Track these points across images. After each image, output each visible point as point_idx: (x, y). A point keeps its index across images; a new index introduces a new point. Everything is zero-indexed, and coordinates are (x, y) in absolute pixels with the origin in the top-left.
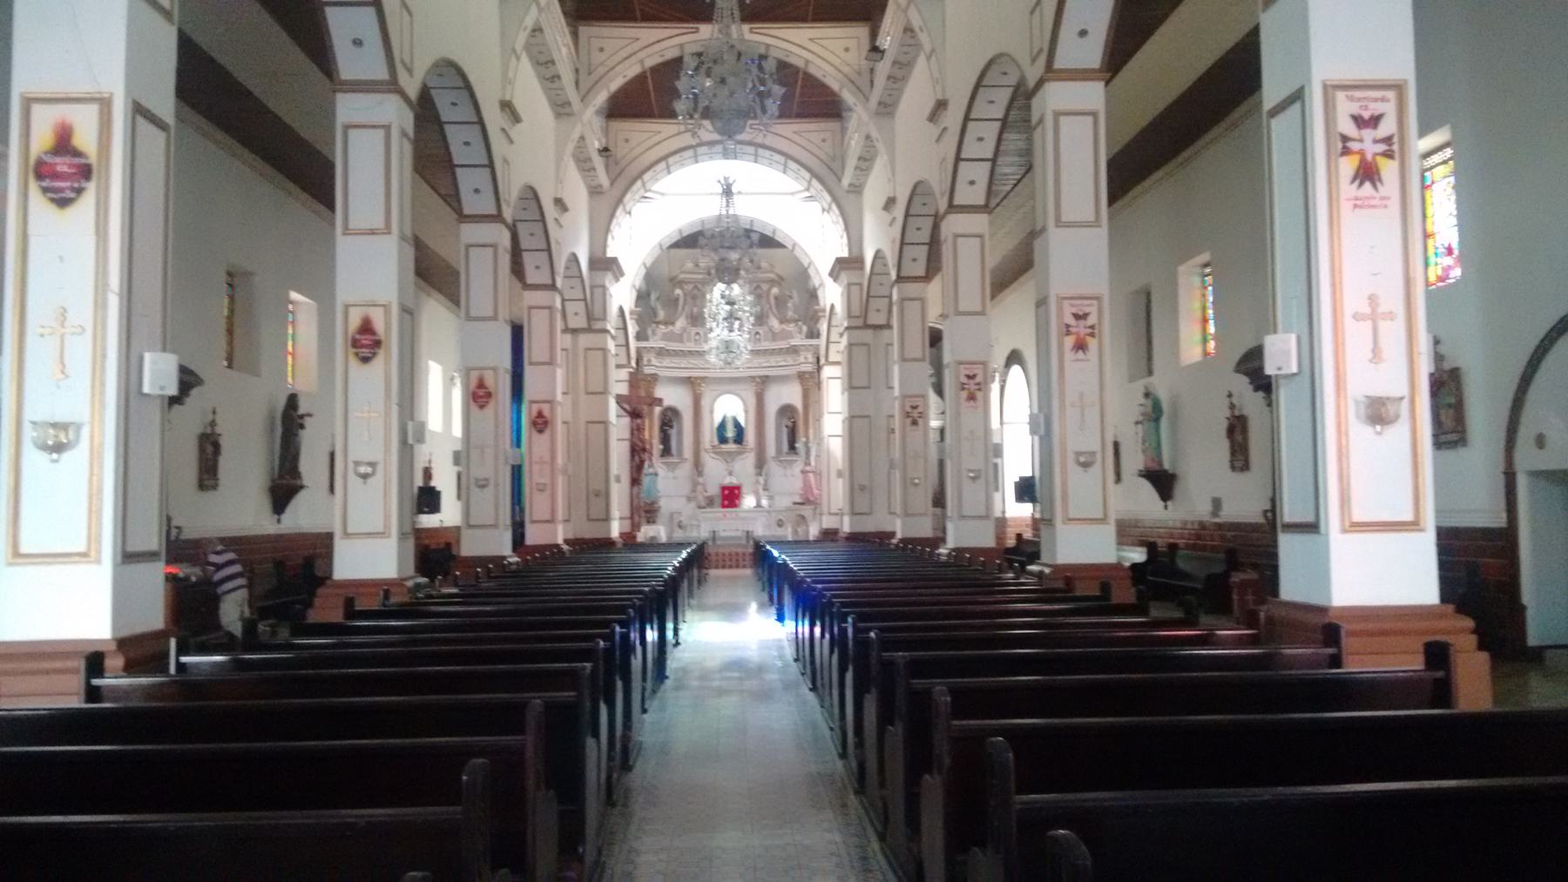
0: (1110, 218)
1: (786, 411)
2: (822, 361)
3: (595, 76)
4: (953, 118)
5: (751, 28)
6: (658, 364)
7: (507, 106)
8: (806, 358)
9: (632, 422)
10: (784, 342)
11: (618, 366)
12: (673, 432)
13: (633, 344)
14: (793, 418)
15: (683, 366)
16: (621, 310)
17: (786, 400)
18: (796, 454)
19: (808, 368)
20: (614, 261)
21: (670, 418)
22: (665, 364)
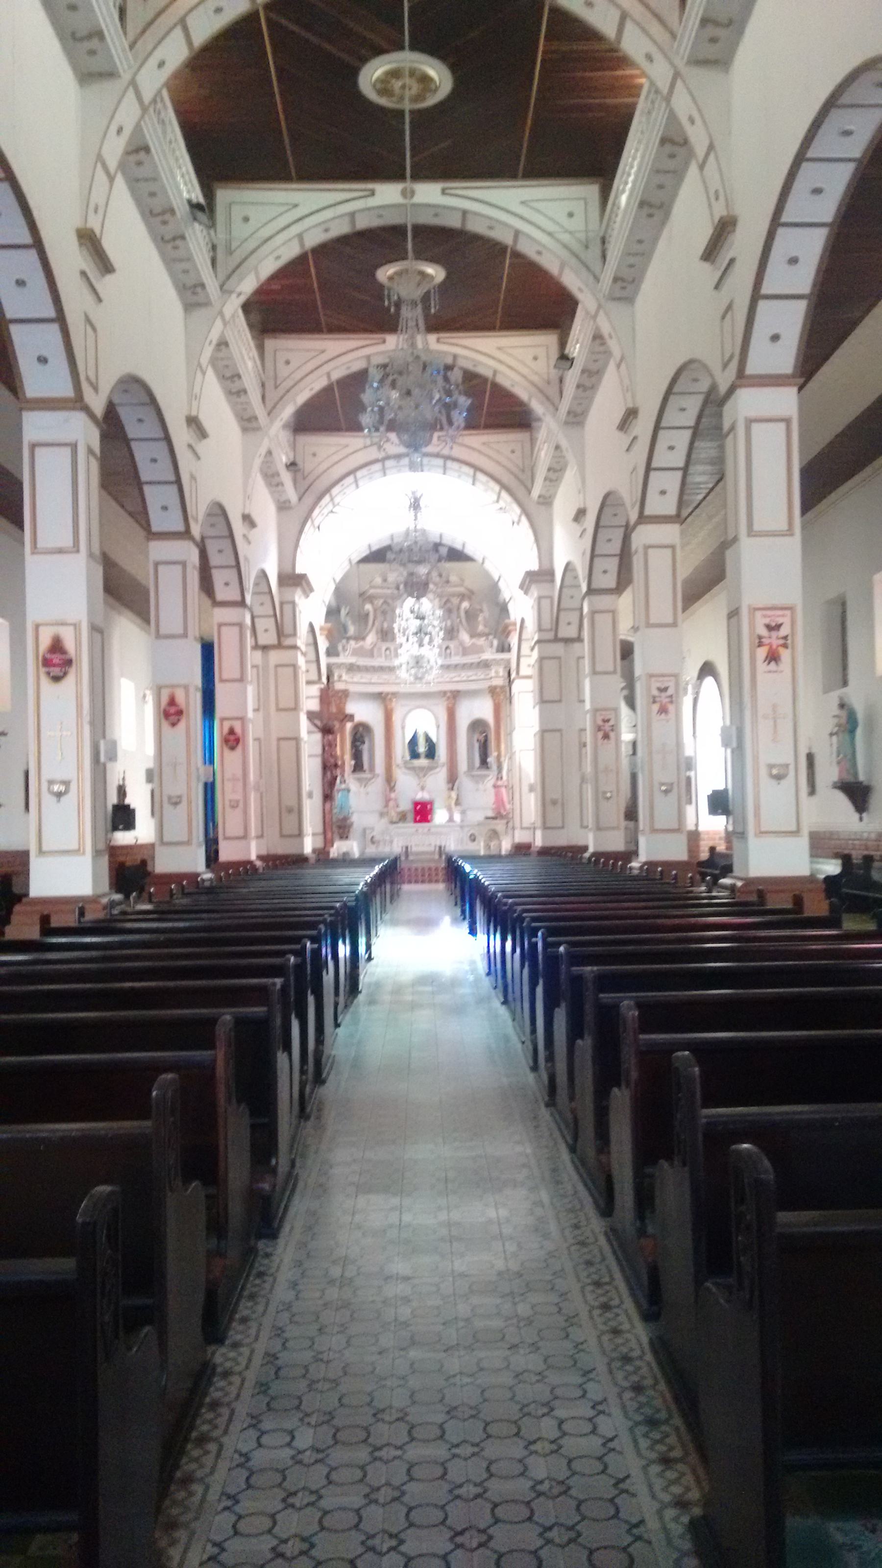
0: (804, 527)
1: (478, 726)
2: (513, 675)
7: (193, 422)
9: (323, 737)
11: (309, 683)
12: (365, 748)
13: (324, 660)
18: (488, 768)
19: (499, 682)
21: (361, 733)
22: (355, 680)
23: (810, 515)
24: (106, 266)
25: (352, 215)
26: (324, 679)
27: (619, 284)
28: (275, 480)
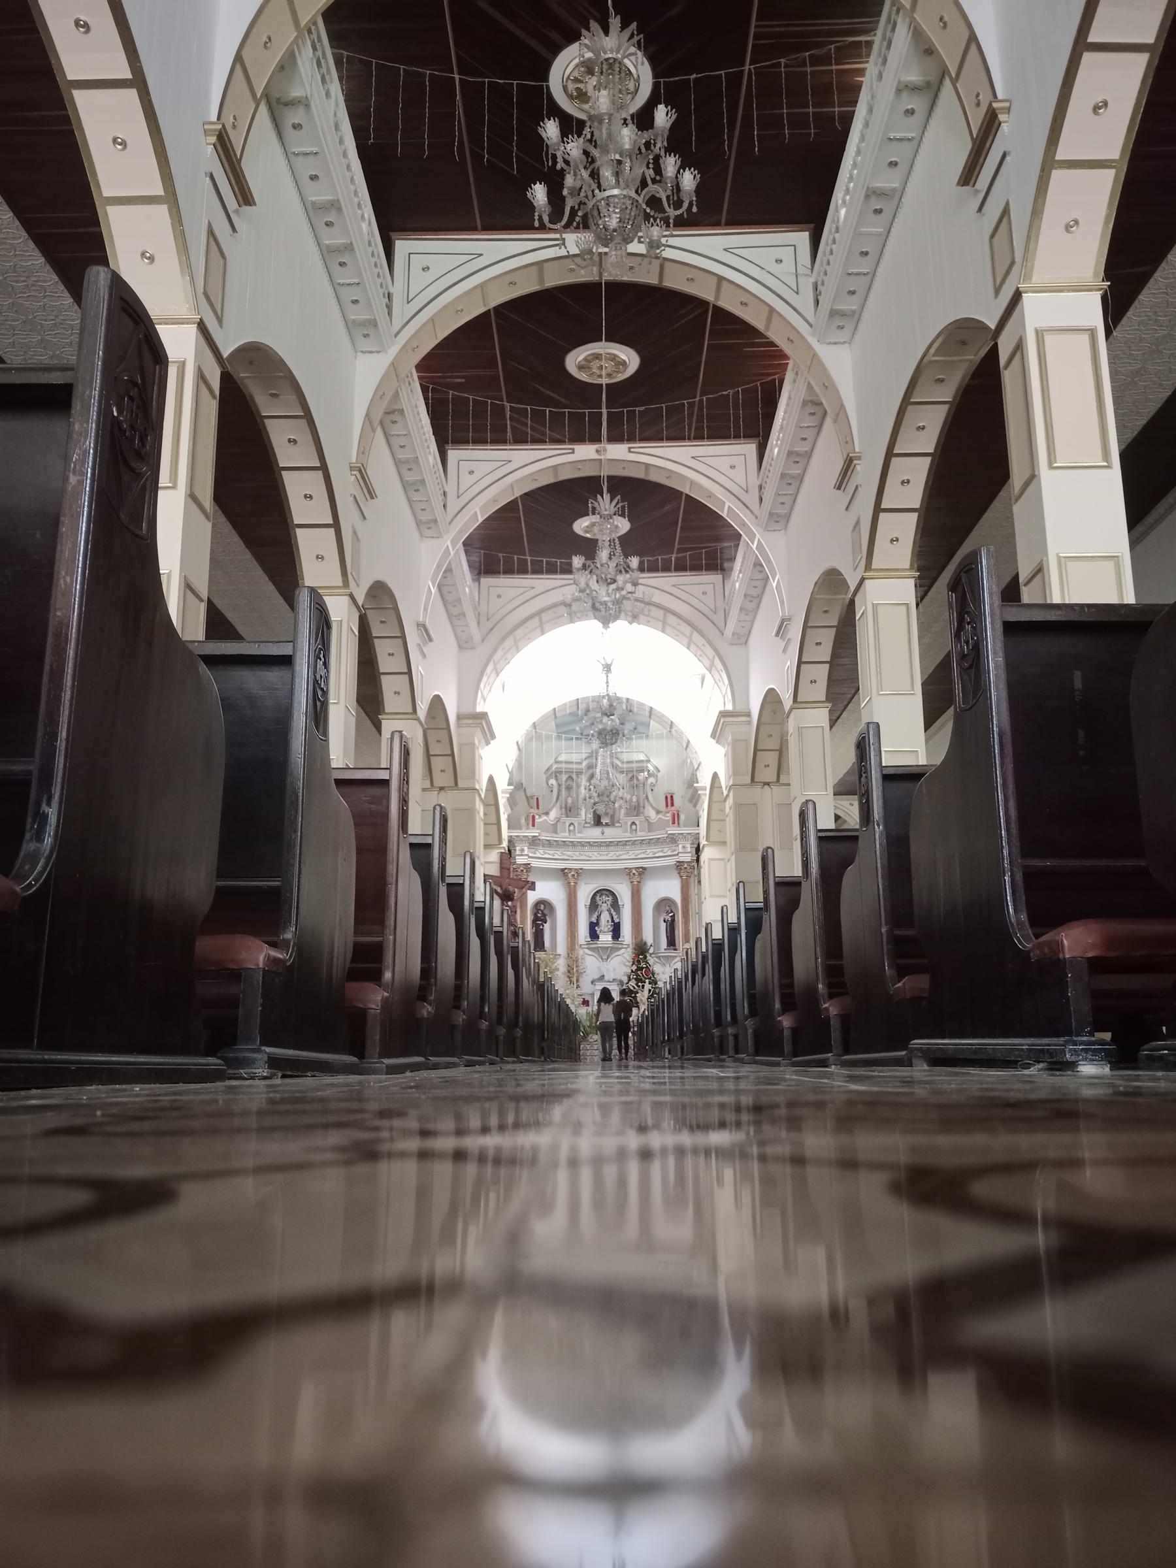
1: (664, 904)
3: (494, 620)
4: (867, 474)
5: (630, 448)
6: (530, 855)
7: (361, 472)
8: (684, 847)
10: (663, 832)
11: (487, 847)
12: (547, 927)
14: (672, 912)
15: (556, 857)
16: (491, 780)
17: (663, 894)
19: (687, 857)
20: (483, 716)
21: (543, 911)
22: (538, 855)
23: (1140, 528)
24: (245, 197)
25: (555, 468)
26: (505, 844)
27: (749, 598)
28: (455, 611)
